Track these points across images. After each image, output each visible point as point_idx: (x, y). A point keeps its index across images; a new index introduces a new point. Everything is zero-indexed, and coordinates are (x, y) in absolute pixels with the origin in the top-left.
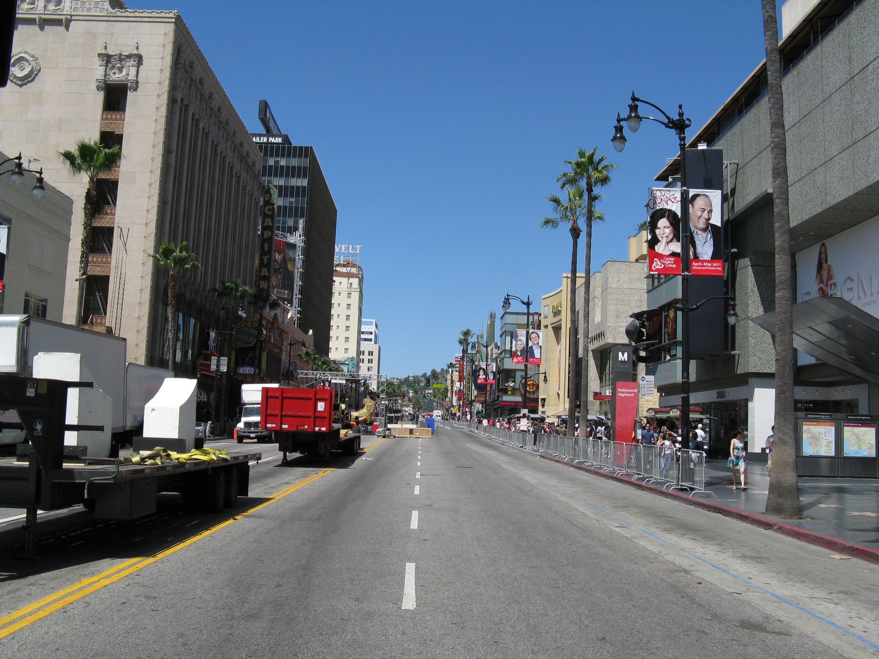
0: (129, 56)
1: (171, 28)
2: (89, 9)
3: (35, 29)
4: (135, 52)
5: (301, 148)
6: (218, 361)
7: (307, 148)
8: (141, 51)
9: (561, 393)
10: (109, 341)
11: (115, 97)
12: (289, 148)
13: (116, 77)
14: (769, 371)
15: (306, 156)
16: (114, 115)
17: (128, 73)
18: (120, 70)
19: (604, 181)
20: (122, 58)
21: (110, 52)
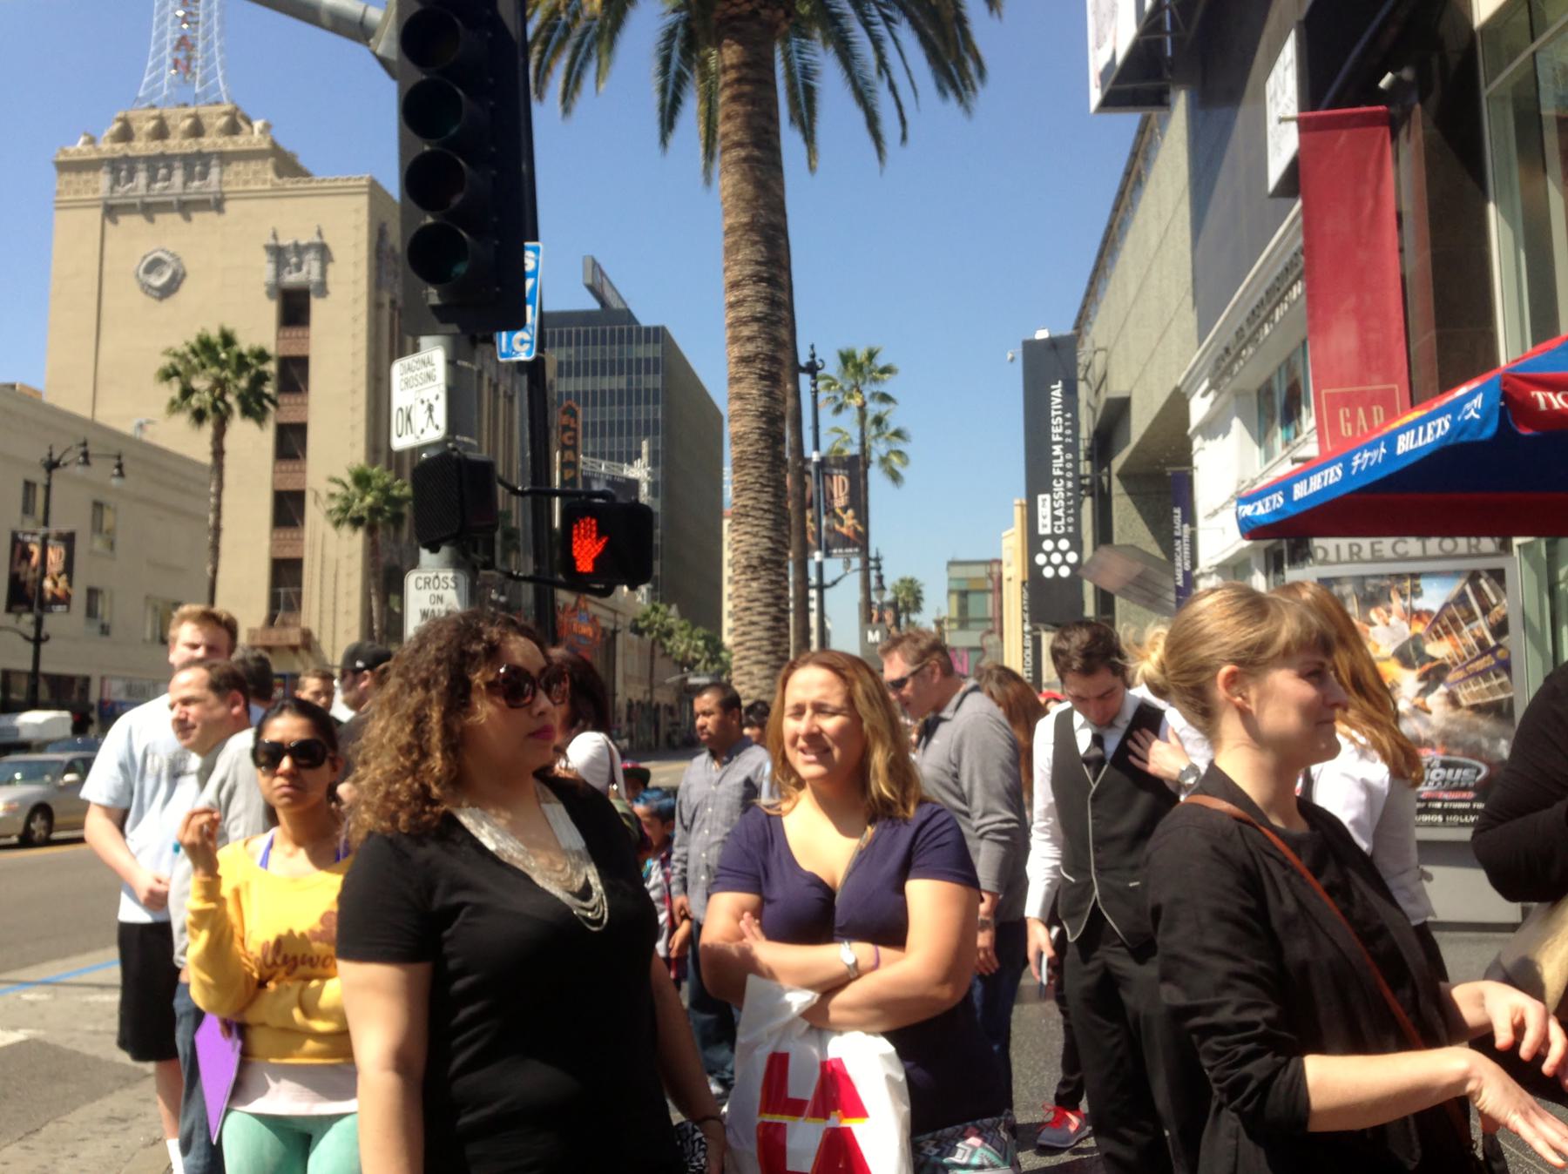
0: (308, 247)
1: (363, 201)
2: (246, 182)
3: (175, 218)
4: (317, 240)
7: (656, 329)
9: (1407, 208)
11: (294, 308)
13: (292, 278)
14: (1116, 529)
15: (656, 341)
16: (295, 332)
17: (310, 271)
18: (299, 268)
19: (228, 340)
20: (299, 250)
21: (285, 241)
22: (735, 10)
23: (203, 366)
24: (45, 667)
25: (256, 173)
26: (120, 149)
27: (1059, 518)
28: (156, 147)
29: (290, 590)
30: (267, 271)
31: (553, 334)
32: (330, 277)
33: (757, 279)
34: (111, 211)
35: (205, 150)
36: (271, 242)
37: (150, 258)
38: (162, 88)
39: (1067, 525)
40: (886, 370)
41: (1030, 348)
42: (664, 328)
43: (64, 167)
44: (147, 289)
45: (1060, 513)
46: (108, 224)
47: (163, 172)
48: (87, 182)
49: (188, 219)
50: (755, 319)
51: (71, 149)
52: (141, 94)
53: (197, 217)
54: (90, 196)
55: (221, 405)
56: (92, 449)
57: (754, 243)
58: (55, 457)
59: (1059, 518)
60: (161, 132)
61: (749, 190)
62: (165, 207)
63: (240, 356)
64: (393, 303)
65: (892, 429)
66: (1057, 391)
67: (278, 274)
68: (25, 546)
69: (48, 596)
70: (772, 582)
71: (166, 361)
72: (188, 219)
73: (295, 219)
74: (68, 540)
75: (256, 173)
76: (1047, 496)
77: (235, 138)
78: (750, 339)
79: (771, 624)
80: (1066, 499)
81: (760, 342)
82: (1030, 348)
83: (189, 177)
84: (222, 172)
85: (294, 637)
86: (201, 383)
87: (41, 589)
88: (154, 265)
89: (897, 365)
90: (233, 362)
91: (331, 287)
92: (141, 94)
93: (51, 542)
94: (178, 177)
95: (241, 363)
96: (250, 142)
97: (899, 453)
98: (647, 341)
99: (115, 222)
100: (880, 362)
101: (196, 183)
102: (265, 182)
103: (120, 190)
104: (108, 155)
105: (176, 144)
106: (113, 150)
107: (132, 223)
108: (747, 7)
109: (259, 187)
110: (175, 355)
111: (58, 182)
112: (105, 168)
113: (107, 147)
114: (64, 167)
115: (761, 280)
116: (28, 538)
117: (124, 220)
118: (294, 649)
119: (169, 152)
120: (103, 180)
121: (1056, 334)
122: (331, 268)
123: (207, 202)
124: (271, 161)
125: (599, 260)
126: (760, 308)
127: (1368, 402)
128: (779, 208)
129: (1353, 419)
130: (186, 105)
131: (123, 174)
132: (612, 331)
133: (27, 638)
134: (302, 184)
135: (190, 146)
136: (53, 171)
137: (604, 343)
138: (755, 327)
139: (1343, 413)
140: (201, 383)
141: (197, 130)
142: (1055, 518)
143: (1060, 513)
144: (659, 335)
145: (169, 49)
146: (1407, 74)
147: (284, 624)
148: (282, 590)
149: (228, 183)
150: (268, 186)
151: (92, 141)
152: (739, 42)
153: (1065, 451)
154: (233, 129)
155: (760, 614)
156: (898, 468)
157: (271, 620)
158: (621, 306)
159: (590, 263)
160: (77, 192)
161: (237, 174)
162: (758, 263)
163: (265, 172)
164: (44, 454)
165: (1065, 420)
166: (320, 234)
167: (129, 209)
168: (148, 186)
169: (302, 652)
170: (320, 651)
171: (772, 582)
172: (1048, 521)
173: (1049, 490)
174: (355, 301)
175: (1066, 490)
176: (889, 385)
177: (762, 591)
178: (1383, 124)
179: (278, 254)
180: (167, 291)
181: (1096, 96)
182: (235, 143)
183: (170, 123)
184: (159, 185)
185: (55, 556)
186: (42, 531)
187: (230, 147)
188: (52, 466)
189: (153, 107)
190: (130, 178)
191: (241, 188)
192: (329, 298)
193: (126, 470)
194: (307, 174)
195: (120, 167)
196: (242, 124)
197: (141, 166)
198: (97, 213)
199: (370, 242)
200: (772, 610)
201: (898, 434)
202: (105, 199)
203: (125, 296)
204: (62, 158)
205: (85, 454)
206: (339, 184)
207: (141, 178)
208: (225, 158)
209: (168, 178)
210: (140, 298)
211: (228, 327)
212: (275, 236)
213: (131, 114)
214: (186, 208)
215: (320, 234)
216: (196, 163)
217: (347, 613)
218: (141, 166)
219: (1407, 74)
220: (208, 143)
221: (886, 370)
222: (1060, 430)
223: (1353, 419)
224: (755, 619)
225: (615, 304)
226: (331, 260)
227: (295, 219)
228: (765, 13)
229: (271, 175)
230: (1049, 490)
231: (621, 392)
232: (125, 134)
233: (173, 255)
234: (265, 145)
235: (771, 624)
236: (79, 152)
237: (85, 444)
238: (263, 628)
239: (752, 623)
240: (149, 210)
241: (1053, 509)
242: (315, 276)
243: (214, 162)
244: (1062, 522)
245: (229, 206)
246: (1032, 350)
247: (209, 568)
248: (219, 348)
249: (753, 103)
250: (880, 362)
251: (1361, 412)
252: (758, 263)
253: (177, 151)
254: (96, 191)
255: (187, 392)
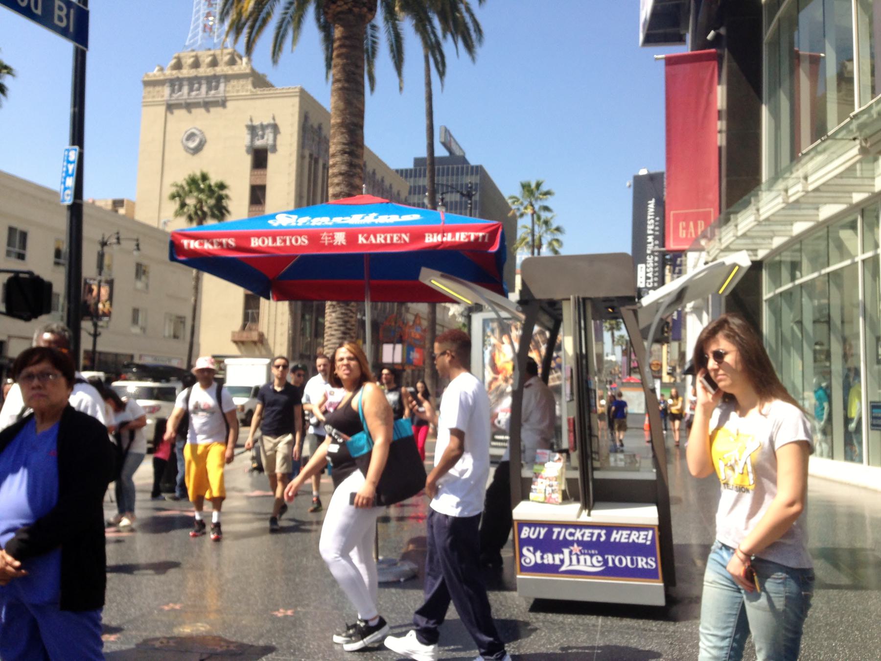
0: (268, 126)
1: (296, 100)
2: (238, 91)
3: (201, 111)
4: (272, 122)
5: (407, 170)
6: (505, 441)
7: (477, 167)
8: (278, 122)
10: (654, 441)
12: (467, 168)
13: (259, 143)
15: (477, 174)
16: (259, 172)
18: (263, 137)
19: (204, 177)
20: (263, 127)
21: (256, 123)
22: (339, 9)
23: (191, 192)
24: (99, 348)
25: (243, 86)
26: (175, 73)
27: (649, 278)
28: (193, 73)
29: (254, 311)
30: (246, 139)
31: (439, 169)
32: (278, 142)
33: (344, 152)
34: (170, 107)
35: (218, 74)
36: (249, 123)
37: (189, 133)
38: (197, 41)
39: (654, 282)
40: (548, 193)
41: (638, 180)
42: (481, 167)
43: (147, 84)
44: (187, 149)
45: (650, 275)
46: (169, 114)
47: (196, 86)
48: (158, 92)
49: (190, 112)
50: (341, 174)
51: (151, 74)
52: (187, 43)
53: (213, 110)
54: (160, 99)
55: (199, 213)
56: (122, 237)
57: (342, 133)
58: (105, 239)
59: (649, 278)
60: (196, 64)
61: (341, 105)
62: (197, 105)
63: (210, 186)
64: (311, 156)
65: (554, 226)
66: (651, 205)
67: (252, 140)
68: (90, 286)
69: (100, 312)
70: (342, 313)
71: (174, 190)
72: (190, 112)
73: (262, 110)
74: (111, 283)
75: (243, 86)
76: (643, 266)
77: (233, 67)
78: (338, 184)
79: (341, 336)
80: (654, 267)
81: (342, 186)
82: (638, 180)
83: (209, 89)
84: (225, 86)
85: (255, 336)
86: (191, 201)
87: (97, 309)
88: (191, 137)
89: (553, 190)
90: (207, 189)
91: (278, 147)
92: (187, 43)
93: (103, 284)
94: (204, 88)
95: (210, 191)
96: (240, 69)
97: (557, 240)
98: (472, 174)
99: (172, 113)
100: (544, 188)
101: (213, 92)
102: (247, 91)
103: (175, 96)
104: (170, 77)
105: (204, 71)
106: (171, 75)
107: (180, 113)
108: (346, 7)
109: (244, 93)
110: (177, 186)
111: (143, 91)
112: (167, 84)
113: (169, 73)
114: (147, 84)
115: (345, 153)
116: (91, 282)
117: (177, 112)
118: (255, 343)
119: (199, 75)
120: (166, 90)
121: (653, 171)
122: (279, 137)
123: (217, 102)
124: (250, 79)
125: (449, 128)
126: (344, 168)
127: (696, 218)
128: (360, 114)
129: (687, 228)
130: (209, 49)
131: (176, 87)
132: (453, 169)
133: (90, 334)
134: (266, 91)
135: (210, 72)
136: (141, 85)
137: (448, 175)
138: (340, 178)
139: (682, 224)
140: (191, 201)
141: (214, 63)
142: (647, 278)
143: (650, 275)
144: (479, 170)
145: (202, 19)
146: (722, 31)
147: (250, 329)
148: (250, 311)
149: (228, 92)
150: (249, 93)
151: (162, 69)
152: (342, 26)
153: (655, 239)
154: (232, 62)
155: (336, 330)
156: (557, 249)
157: (244, 327)
158: (461, 154)
159: (443, 129)
160: (154, 97)
161: (234, 86)
162: (344, 144)
163: (247, 86)
164: (100, 238)
165: (656, 221)
166: (274, 119)
167: (178, 106)
168: (189, 94)
169: (259, 345)
170: (268, 344)
171: (342, 313)
172: (643, 279)
173: (644, 261)
174: (291, 155)
175: (654, 262)
176: (549, 202)
177: (337, 318)
178: (714, 60)
179: (252, 130)
180: (197, 150)
181: (641, 37)
182: (233, 70)
183: (201, 59)
184: (194, 93)
185: (104, 291)
186: (99, 278)
187: (230, 72)
188: (104, 244)
189: (193, 51)
190: (180, 90)
191: (235, 94)
192: (277, 153)
193: (141, 247)
194: (272, 86)
195: (175, 84)
196: (237, 59)
197: (185, 83)
198: (163, 109)
199: (299, 121)
200: (342, 328)
201: (558, 229)
202: (167, 101)
203: (176, 152)
204: (146, 79)
205: (118, 239)
206: (291, 90)
207: (185, 89)
208: (228, 78)
209: (199, 89)
210: (184, 154)
211: (205, 170)
212: (251, 120)
213: (182, 55)
214: (207, 105)
215: (274, 119)
216: (213, 81)
217: (282, 324)
218: (185, 83)
219: (722, 31)
220: (222, 69)
221: (548, 193)
222: (652, 227)
223: (687, 228)
224: (333, 333)
225: (458, 153)
226: (279, 133)
227: (262, 110)
228: (356, 10)
229: (250, 87)
230: (644, 261)
231: (456, 202)
232: (178, 66)
233: (200, 131)
234: (248, 71)
235: (341, 336)
236: (155, 75)
237: (118, 233)
238: (240, 332)
239: (332, 335)
240: (189, 106)
241: (647, 273)
242: (271, 142)
243: (222, 80)
244: (651, 280)
245: (229, 104)
246: (639, 181)
247: (193, 299)
248: (200, 182)
249: (347, 58)
250: (544, 188)
251: (691, 224)
252: (344, 144)
253: (203, 74)
254: (163, 96)
255: (183, 205)
